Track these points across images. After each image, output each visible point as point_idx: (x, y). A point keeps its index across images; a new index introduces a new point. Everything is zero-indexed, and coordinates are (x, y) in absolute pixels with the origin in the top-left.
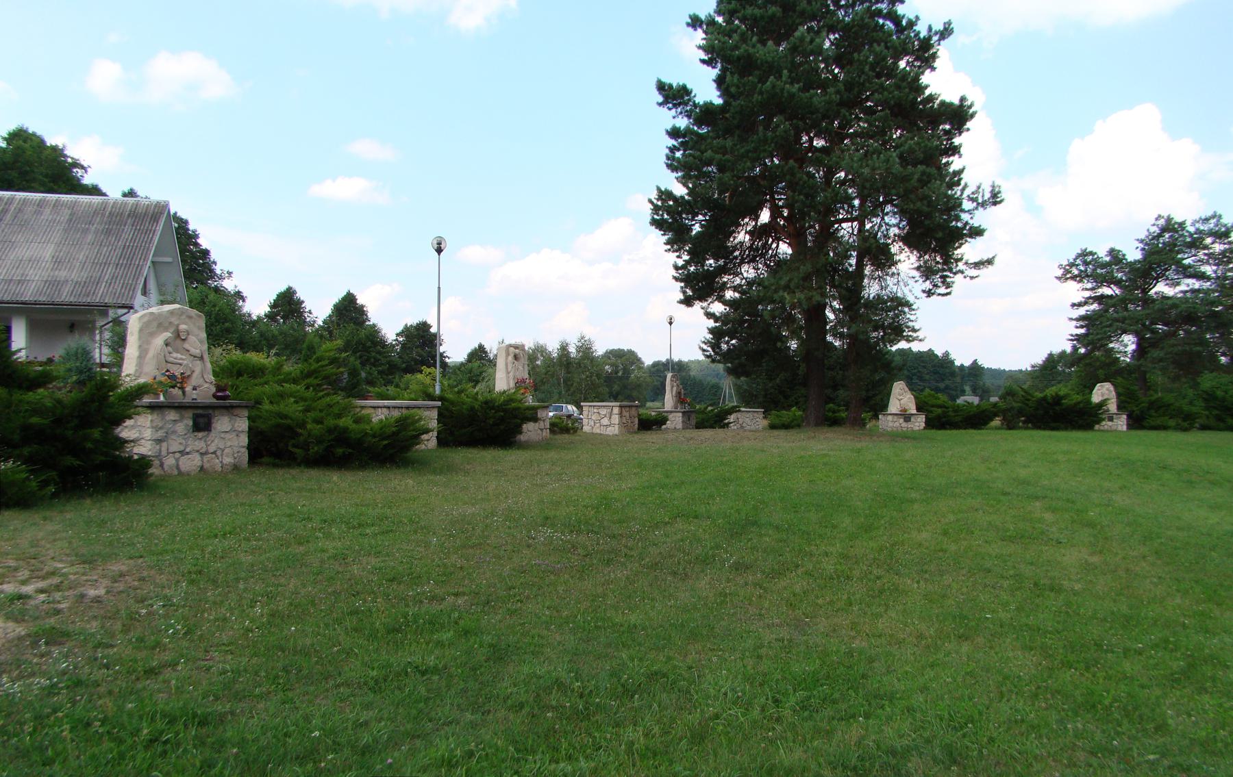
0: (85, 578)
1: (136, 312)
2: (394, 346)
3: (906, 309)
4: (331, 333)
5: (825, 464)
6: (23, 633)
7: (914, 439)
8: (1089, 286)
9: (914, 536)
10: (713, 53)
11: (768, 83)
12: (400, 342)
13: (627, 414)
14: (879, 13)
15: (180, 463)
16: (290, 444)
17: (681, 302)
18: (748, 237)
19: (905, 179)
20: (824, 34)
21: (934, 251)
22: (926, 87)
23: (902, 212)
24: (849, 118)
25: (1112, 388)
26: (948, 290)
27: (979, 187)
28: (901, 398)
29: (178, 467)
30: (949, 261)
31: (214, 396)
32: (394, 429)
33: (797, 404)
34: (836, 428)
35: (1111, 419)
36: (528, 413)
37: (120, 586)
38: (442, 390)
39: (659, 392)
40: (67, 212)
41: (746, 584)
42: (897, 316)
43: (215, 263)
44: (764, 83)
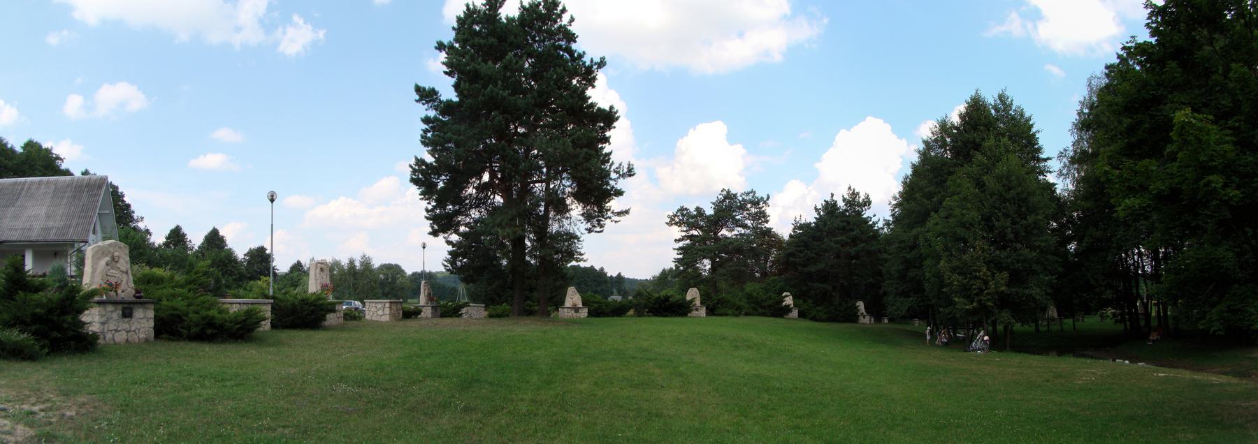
0: (64, 404)
1: (89, 246)
2: (243, 263)
3: (576, 241)
4: (203, 255)
5: (523, 341)
6: (33, 434)
7: (581, 323)
8: (685, 229)
9: (577, 386)
10: (453, 67)
11: (488, 89)
12: (246, 260)
13: (395, 308)
14: (560, 47)
15: (115, 337)
16: (179, 326)
17: (430, 233)
18: (474, 191)
19: (575, 156)
20: (525, 58)
21: (593, 204)
22: (589, 98)
23: (573, 178)
24: (540, 115)
25: (698, 292)
26: (601, 229)
27: (620, 165)
28: (573, 297)
29: (114, 340)
30: (602, 211)
31: (135, 296)
32: (244, 318)
33: (506, 301)
34: (532, 318)
35: (697, 310)
36: (330, 307)
37: (83, 411)
38: (274, 292)
39: (416, 293)
40: (53, 186)
41: (471, 420)
42: (570, 245)
43: (133, 212)
44: (485, 89)
